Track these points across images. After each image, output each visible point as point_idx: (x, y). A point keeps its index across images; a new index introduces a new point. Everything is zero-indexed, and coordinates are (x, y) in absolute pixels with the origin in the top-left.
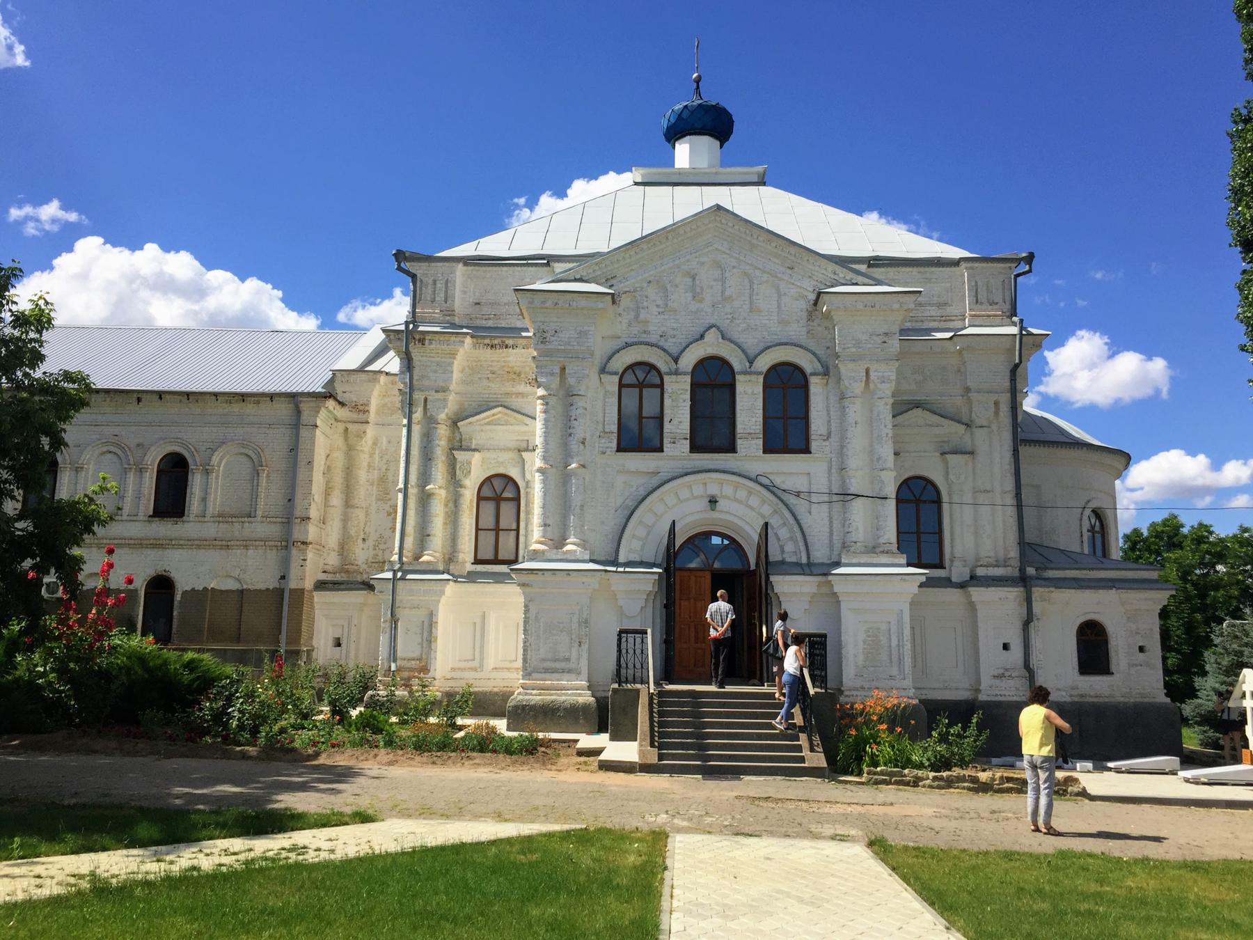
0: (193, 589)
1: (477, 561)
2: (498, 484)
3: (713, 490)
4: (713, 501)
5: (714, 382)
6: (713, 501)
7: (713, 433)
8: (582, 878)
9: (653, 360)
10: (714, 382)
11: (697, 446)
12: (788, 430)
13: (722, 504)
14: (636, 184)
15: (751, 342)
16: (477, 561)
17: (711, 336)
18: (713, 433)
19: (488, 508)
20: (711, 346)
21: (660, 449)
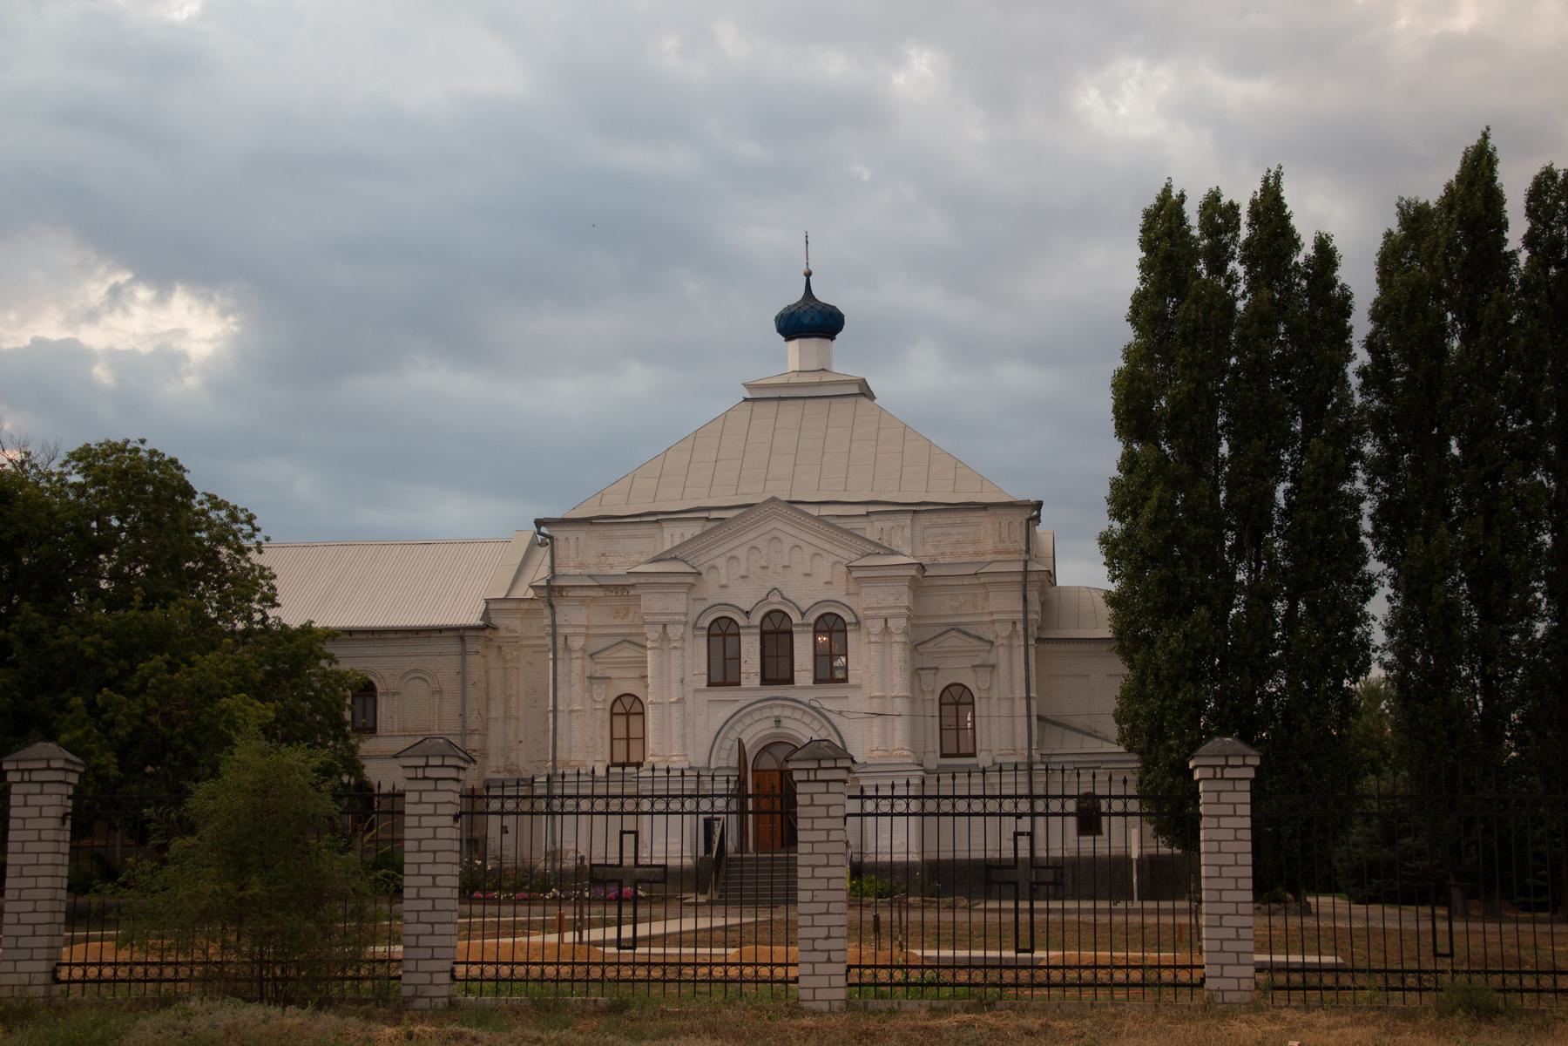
0: (1135, 317)
1: (943, 756)
2: (627, 701)
3: (777, 712)
4: (778, 722)
5: (776, 635)
6: (778, 722)
7: (776, 672)
8: (345, 801)
9: (711, 618)
10: (776, 635)
11: (765, 680)
12: (829, 673)
13: (785, 723)
14: (746, 400)
15: (804, 606)
16: (943, 756)
17: (776, 598)
18: (776, 672)
19: (620, 722)
20: (775, 603)
21: (739, 684)
